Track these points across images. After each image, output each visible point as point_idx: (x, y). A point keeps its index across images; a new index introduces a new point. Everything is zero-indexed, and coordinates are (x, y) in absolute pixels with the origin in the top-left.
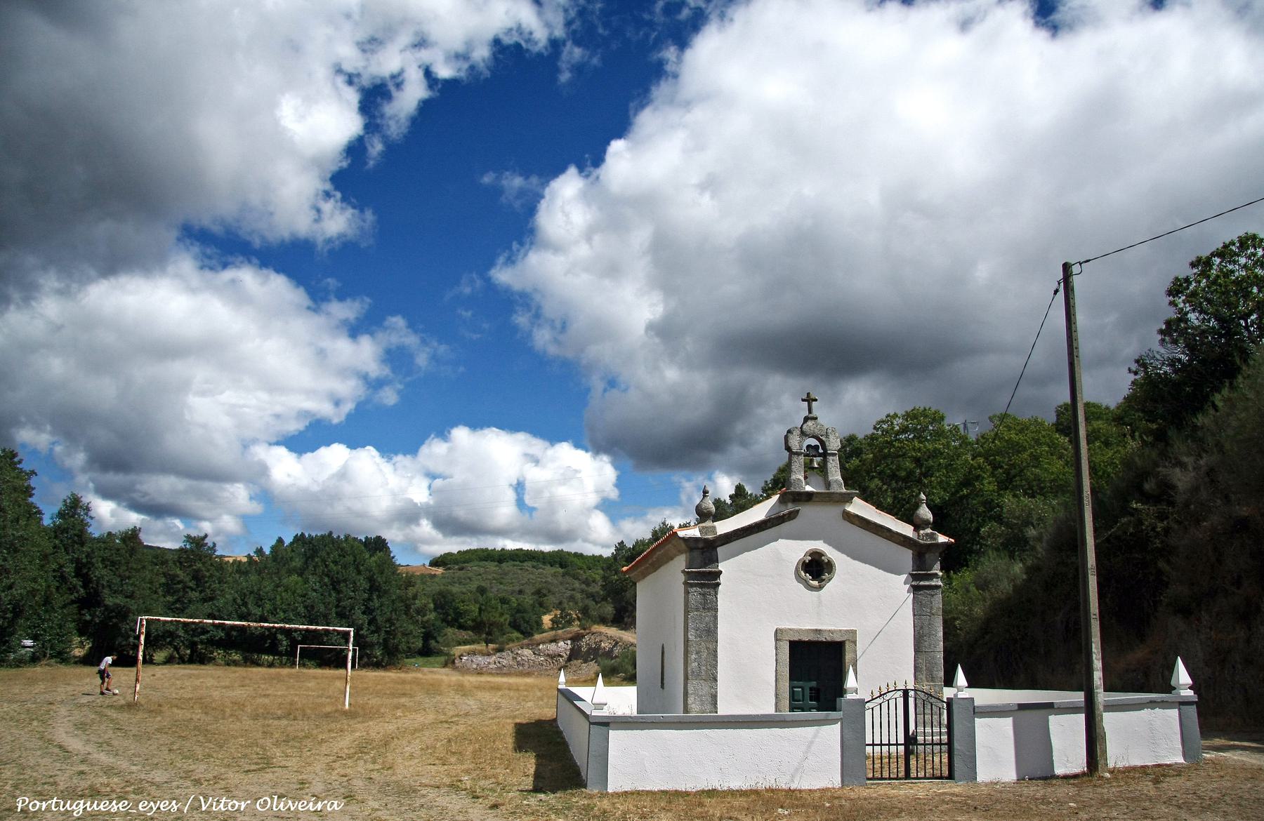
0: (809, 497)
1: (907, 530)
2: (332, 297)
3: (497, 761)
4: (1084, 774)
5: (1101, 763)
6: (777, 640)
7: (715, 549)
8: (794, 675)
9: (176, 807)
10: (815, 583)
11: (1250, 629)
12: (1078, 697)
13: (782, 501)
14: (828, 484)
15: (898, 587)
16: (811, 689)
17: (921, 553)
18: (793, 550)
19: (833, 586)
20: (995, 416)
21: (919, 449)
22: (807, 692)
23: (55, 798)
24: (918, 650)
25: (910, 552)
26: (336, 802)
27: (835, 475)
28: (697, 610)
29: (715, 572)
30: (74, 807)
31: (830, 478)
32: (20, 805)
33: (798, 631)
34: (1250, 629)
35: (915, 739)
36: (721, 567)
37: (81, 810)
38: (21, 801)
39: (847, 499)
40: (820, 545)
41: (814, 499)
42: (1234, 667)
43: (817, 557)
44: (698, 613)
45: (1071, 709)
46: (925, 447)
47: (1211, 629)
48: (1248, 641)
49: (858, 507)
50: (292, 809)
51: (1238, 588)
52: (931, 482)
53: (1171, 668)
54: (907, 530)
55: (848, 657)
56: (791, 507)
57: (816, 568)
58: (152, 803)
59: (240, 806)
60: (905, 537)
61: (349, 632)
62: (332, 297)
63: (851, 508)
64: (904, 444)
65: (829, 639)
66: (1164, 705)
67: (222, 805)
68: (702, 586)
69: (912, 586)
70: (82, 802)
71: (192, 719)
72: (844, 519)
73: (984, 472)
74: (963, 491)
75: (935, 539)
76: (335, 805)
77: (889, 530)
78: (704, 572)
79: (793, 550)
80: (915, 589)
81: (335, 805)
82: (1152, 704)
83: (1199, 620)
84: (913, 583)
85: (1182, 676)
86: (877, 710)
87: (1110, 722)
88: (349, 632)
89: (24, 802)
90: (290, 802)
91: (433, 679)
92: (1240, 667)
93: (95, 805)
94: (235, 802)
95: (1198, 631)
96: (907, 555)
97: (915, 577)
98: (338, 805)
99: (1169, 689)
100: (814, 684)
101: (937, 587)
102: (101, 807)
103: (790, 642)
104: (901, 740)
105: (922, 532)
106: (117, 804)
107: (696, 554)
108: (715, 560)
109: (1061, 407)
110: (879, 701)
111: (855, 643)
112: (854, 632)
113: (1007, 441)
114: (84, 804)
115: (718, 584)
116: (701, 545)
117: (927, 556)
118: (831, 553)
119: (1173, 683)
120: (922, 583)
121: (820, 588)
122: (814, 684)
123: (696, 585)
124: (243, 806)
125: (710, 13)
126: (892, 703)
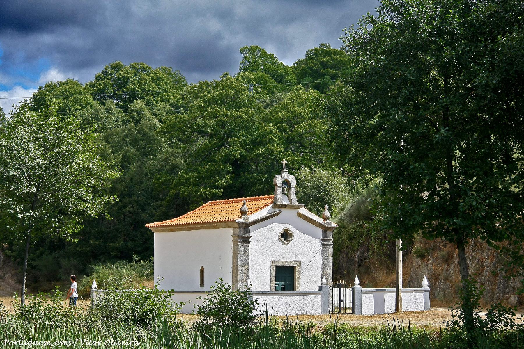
0: (285, 206)
1: (320, 220)
4: (394, 313)
5: (400, 309)
6: (271, 265)
7: (248, 227)
10: (285, 242)
11: (448, 266)
12: (394, 289)
13: (273, 207)
14: (291, 201)
15: (317, 243)
16: (282, 285)
17: (326, 230)
18: (277, 228)
19: (293, 243)
20: (245, 48)
21: (227, 115)
22: (281, 286)
24: (323, 271)
27: (293, 196)
28: (242, 252)
29: (247, 237)
31: (292, 198)
33: (279, 262)
34: (448, 266)
35: (343, 300)
36: (251, 234)
39: (299, 207)
40: (288, 226)
41: (287, 207)
42: (440, 281)
43: (286, 231)
44: (242, 254)
45: (392, 292)
46: (231, 113)
47: (432, 265)
48: (447, 270)
49: (303, 211)
51: (445, 248)
52: (234, 141)
53: (422, 278)
54: (320, 220)
57: (286, 236)
60: (320, 224)
64: (216, 110)
65: (290, 265)
68: (244, 242)
69: (322, 244)
72: (297, 215)
73: (275, 137)
74: (258, 150)
75: (331, 225)
77: (315, 221)
78: (243, 237)
79: (277, 228)
80: (323, 245)
82: (416, 291)
83: (428, 260)
84: (322, 243)
85: (425, 282)
92: (443, 281)
95: (427, 265)
96: (320, 231)
97: (323, 240)
99: (421, 286)
100: (283, 283)
101: (331, 245)
103: (277, 267)
104: (339, 301)
105: (326, 221)
108: (248, 232)
109: (311, 51)
111: (300, 267)
113: (291, 112)
115: (250, 242)
116: (244, 226)
117: (328, 232)
118: (292, 230)
119: (422, 284)
120: (326, 243)
121: (288, 244)
122: (283, 283)
123: (241, 242)
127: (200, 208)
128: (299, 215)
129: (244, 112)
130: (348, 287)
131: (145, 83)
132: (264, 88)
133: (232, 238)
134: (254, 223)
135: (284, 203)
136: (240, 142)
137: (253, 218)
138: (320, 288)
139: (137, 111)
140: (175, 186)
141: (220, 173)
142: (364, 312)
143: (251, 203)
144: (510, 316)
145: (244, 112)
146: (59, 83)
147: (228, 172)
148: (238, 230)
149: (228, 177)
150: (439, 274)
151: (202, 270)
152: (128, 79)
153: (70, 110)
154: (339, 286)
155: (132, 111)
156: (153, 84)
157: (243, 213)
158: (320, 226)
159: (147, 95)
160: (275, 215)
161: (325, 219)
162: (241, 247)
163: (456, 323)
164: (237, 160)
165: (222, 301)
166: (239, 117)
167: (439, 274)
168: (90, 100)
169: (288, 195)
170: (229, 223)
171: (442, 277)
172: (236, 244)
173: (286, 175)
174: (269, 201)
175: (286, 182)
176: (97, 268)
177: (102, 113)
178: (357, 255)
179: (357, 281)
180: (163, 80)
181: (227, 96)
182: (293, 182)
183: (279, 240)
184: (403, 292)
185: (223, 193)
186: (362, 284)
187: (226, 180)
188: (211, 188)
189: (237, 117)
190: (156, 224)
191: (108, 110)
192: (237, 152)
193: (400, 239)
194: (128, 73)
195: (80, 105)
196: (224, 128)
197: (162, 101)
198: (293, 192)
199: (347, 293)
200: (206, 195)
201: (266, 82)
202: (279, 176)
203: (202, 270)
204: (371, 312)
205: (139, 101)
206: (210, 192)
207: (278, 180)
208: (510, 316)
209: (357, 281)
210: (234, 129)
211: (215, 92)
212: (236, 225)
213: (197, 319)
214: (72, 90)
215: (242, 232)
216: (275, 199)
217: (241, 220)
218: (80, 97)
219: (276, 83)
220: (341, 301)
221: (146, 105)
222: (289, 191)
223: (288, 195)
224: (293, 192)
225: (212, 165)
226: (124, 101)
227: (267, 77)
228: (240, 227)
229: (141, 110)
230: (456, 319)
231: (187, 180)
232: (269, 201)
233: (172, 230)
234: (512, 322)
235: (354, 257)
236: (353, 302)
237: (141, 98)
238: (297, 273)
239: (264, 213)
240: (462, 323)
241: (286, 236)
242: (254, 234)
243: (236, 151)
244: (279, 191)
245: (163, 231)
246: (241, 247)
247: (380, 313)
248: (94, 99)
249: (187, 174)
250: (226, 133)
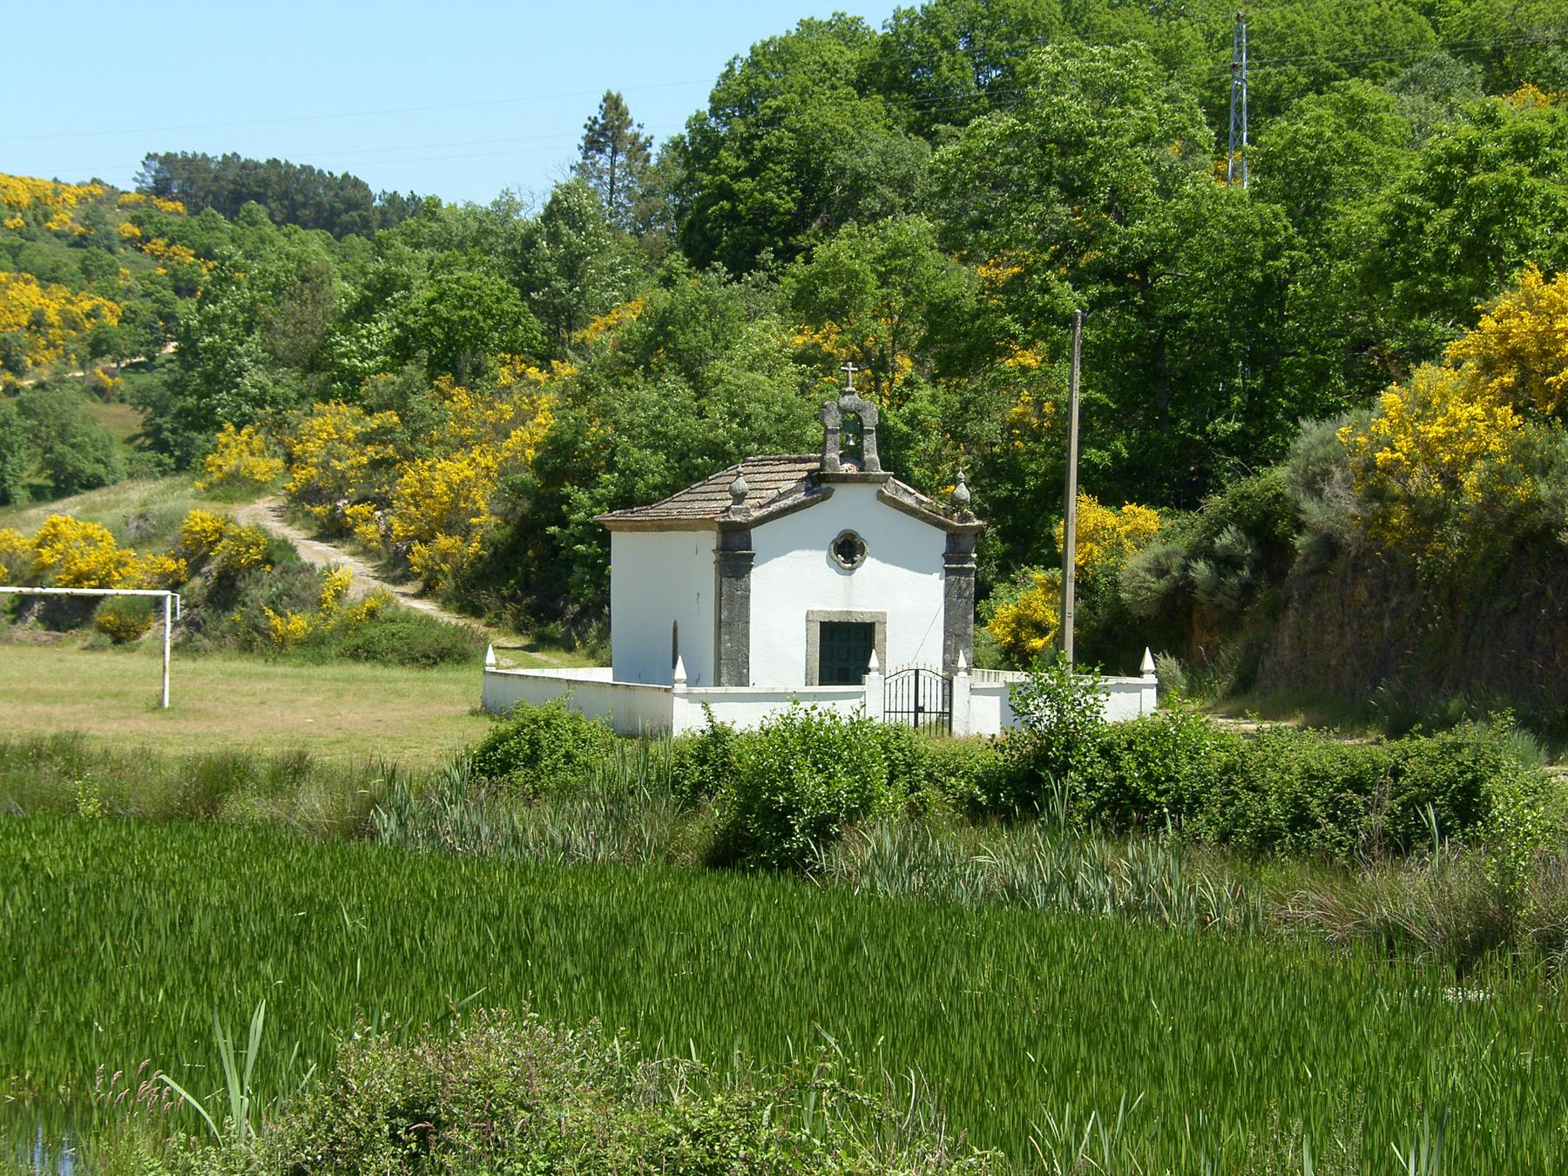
0: (845, 479)
2: (262, 770)
3: (781, 784)
6: (808, 621)
25: (945, 533)
27: (872, 455)
35: (923, 708)
39: (885, 480)
55: (878, 638)
61: (165, 597)
62: (262, 770)
86: (893, 685)
88: (165, 597)
91: (409, 608)
104: (912, 709)
110: (895, 677)
112: (884, 614)
121: (852, 569)
125: (268, 760)
126: (906, 680)
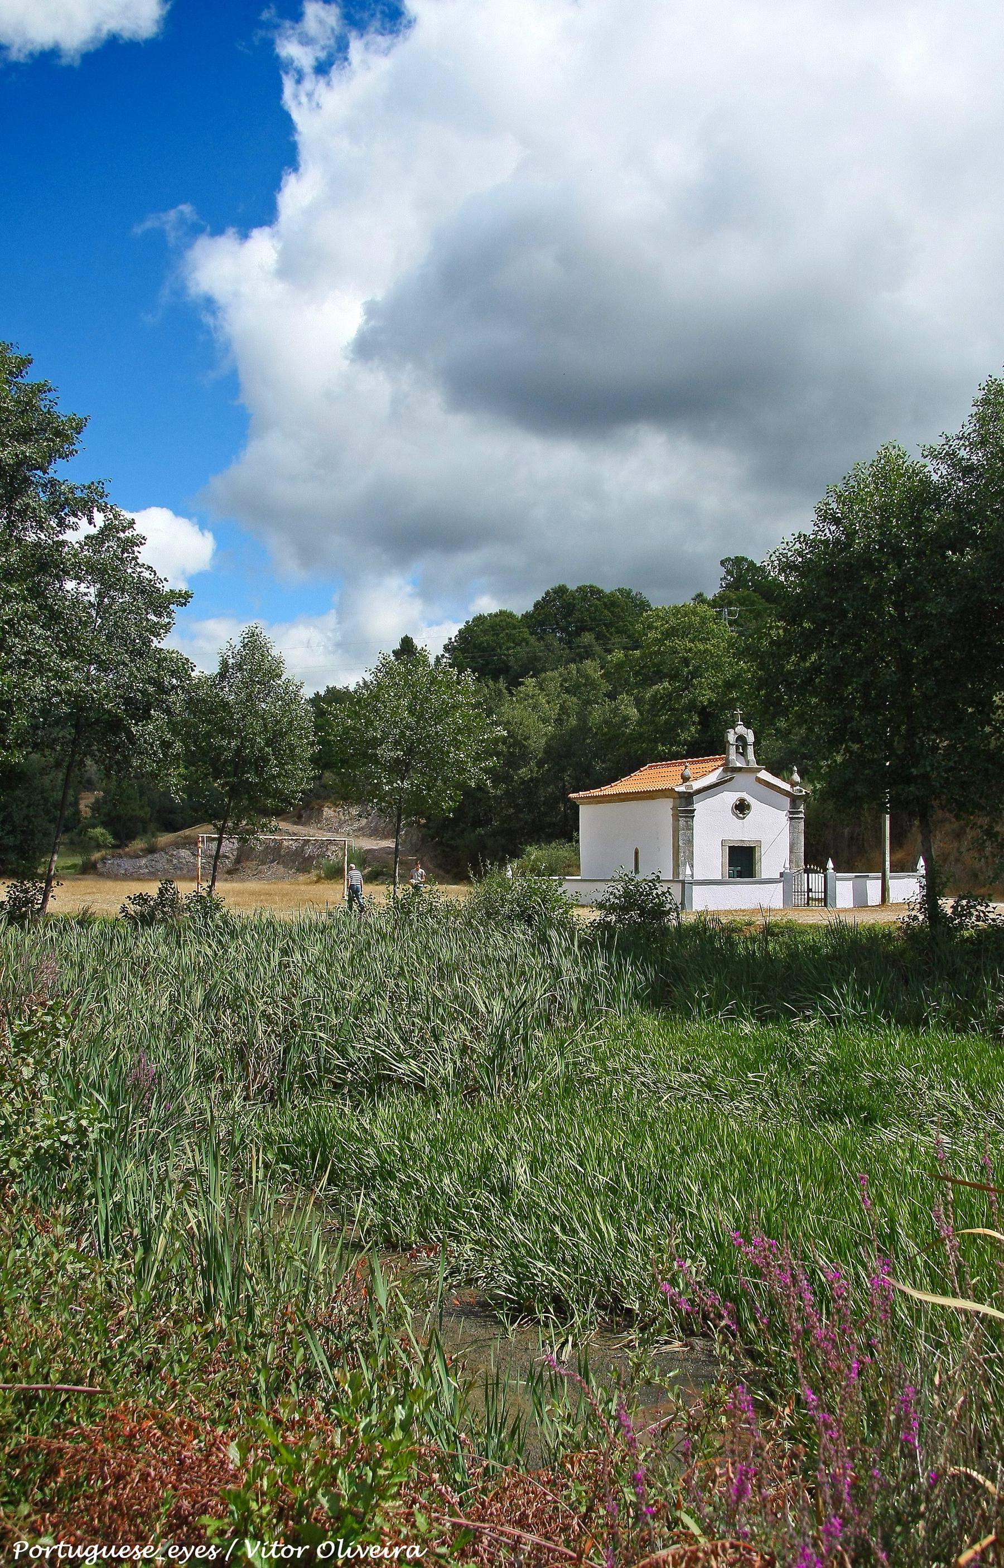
0: (740, 769)
1: (787, 787)
8: (731, 864)
9: (214, 1554)
14: (748, 762)
17: (794, 800)
19: (750, 817)
20: (728, 559)
21: (690, 649)
23: (62, 1542)
24: (791, 852)
26: (417, 1548)
30: (86, 1553)
32: (17, 1551)
36: (695, 806)
37: (95, 1557)
38: (19, 1547)
39: (759, 770)
40: (744, 795)
45: (877, 878)
49: (765, 775)
50: (362, 1556)
54: (787, 787)
56: (729, 775)
57: (742, 808)
58: (185, 1549)
59: (296, 1552)
63: (760, 775)
66: (913, 877)
67: (273, 1551)
68: (686, 817)
70: (96, 1547)
71: (416, 887)
76: (416, 1552)
79: (729, 798)
80: (791, 819)
81: (416, 1552)
87: (892, 883)
89: (22, 1547)
90: (359, 1547)
93: (112, 1551)
94: (289, 1547)
97: (791, 813)
98: (420, 1552)
99: (916, 871)
102: (121, 1553)
106: (140, 1550)
107: (683, 800)
114: (99, 1549)
118: (750, 800)
124: (300, 1551)
127: (637, 773)
128: (759, 780)
129: (713, 645)
130: (816, 872)
131: (596, 611)
132: (751, 611)
133: (671, 812)
134: (699, 791)
135: (738, 765)
136: (708, 684)
137: (697, 785)
138: (782, 875)
139: (585, 647)
140: (626, 742)
141: (683, 725)
142: (840, 904)
143: (695, 766)
144: (983, 908)
145: (713, 645)
146: (490, 615)
147: (694, 723)
148: (678, 801)
149: (693, 729)
150: (949, 854)
151: (637, 853)
152: (574, 605)
153: (501, 648)
154: (807, 871)
155: (579, 647)
156: (606, 612)
157: (685, 779)
158: (787, 793)
159: (598, 626)
160: (726, 781)
161: (793, 784)
162: (682, 822)
163: (915, 918)
164: (704, 708)
165: (627, 894)
166: (706, 651)
167: (949, 854)
168: (527, 635)
169: (743, 754)
170: (667, 793)
171: (952, 858)
172: (676, 818)
173: (741, 729)
174: (720, 763)
175: (741, 738)
176: (529, 849)
177: (541, 651)
178: (846, 831)
179: (830, 865)
180: (618, 606)
181: (691, 625)
182: (751, 738)
183: (734, 814)
184: (891, 878)
185: (687, 751)
186: (836, 869)
187: (690, 733)
188: (672, 745)
189: (704, 652)
190: (587, 793)
191: (548, 647)
192: (706, 696)
193: (390, 843)
194: (574, 599)
195: (514, 642)
196: (688, 667)
197: (617, 633)
198: (750, 750)
199: (816, 880)
200: (665, 753)
201: (753, 603)
202: (731, 731)
203: (637, 853)
204: (850, 905)
205: (587, 634)
206: (670, 750)
207: (731, 737)
208: (983, 908)
209: (830, 865)
210: (700, 666)
211: (673, 622)
212: (677, 796)
213: (597, 915)
214: (504, 623)
215: (684, 804)
216: (727, 761)
217: (682, 789)
218: (514, 632)
219: (767, 605)
220: (809, 890)
221: (597, 639)
222: (745, 748)
223: (743, 754)
224: (750, 750)
225: (672, 714)
226: (569, 634)
227: (755, 597)
228: (680, 798)
229: (590, 646)
230: (913, 913)
231: (641, 735)
232: (720, 763)
233: (623, 800)
234: (986, 916)
235: (843, 833)
236: (825, 892)
237: (590, 630)
238: (757, 855)
239: (712, 778)
240: (921, 917)
241: (742, 808)
242: (701, 807)
243: (704, 695)
244: (732, 750)
245: (590, 803)
246: (682, 822)
247: (861, 902)
248: (531, 634)
249: (641, 727)
250: (689, 672)
